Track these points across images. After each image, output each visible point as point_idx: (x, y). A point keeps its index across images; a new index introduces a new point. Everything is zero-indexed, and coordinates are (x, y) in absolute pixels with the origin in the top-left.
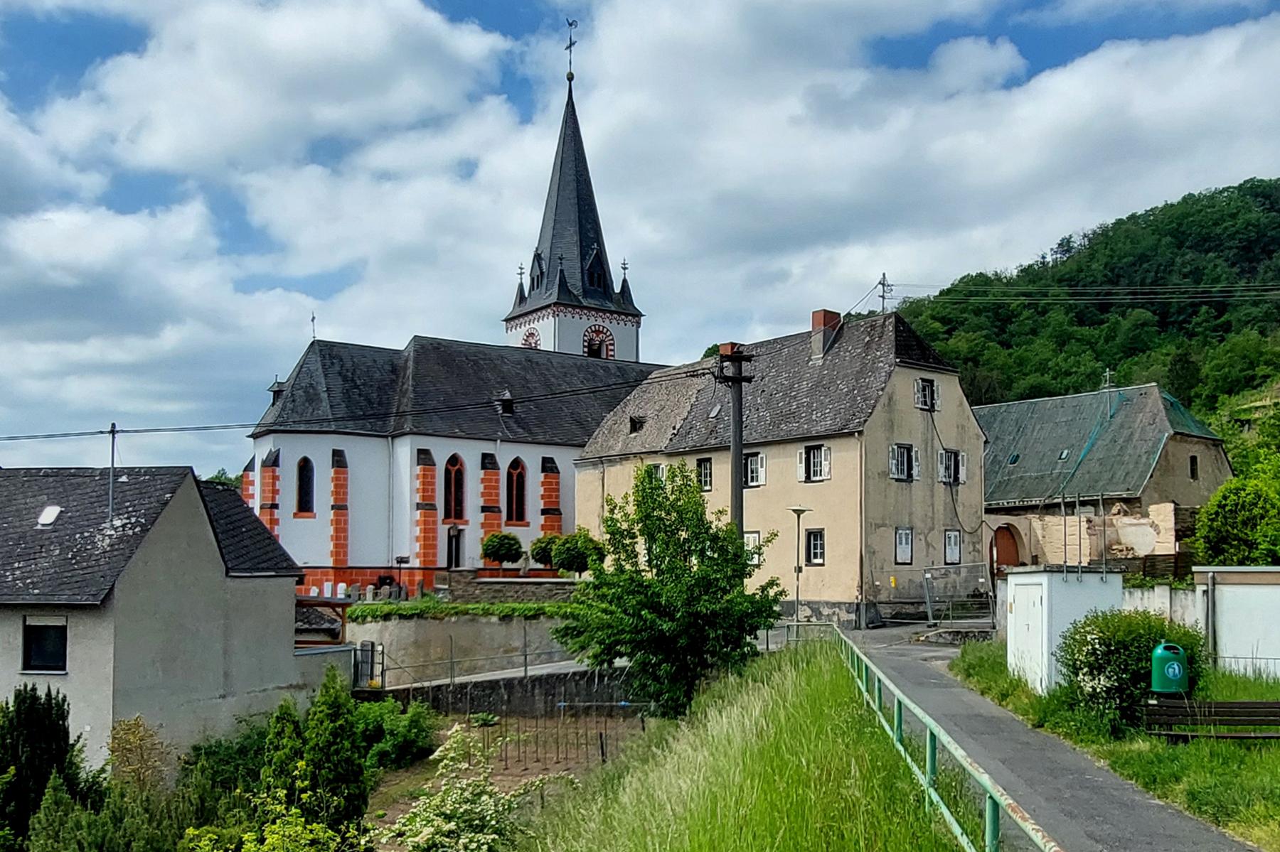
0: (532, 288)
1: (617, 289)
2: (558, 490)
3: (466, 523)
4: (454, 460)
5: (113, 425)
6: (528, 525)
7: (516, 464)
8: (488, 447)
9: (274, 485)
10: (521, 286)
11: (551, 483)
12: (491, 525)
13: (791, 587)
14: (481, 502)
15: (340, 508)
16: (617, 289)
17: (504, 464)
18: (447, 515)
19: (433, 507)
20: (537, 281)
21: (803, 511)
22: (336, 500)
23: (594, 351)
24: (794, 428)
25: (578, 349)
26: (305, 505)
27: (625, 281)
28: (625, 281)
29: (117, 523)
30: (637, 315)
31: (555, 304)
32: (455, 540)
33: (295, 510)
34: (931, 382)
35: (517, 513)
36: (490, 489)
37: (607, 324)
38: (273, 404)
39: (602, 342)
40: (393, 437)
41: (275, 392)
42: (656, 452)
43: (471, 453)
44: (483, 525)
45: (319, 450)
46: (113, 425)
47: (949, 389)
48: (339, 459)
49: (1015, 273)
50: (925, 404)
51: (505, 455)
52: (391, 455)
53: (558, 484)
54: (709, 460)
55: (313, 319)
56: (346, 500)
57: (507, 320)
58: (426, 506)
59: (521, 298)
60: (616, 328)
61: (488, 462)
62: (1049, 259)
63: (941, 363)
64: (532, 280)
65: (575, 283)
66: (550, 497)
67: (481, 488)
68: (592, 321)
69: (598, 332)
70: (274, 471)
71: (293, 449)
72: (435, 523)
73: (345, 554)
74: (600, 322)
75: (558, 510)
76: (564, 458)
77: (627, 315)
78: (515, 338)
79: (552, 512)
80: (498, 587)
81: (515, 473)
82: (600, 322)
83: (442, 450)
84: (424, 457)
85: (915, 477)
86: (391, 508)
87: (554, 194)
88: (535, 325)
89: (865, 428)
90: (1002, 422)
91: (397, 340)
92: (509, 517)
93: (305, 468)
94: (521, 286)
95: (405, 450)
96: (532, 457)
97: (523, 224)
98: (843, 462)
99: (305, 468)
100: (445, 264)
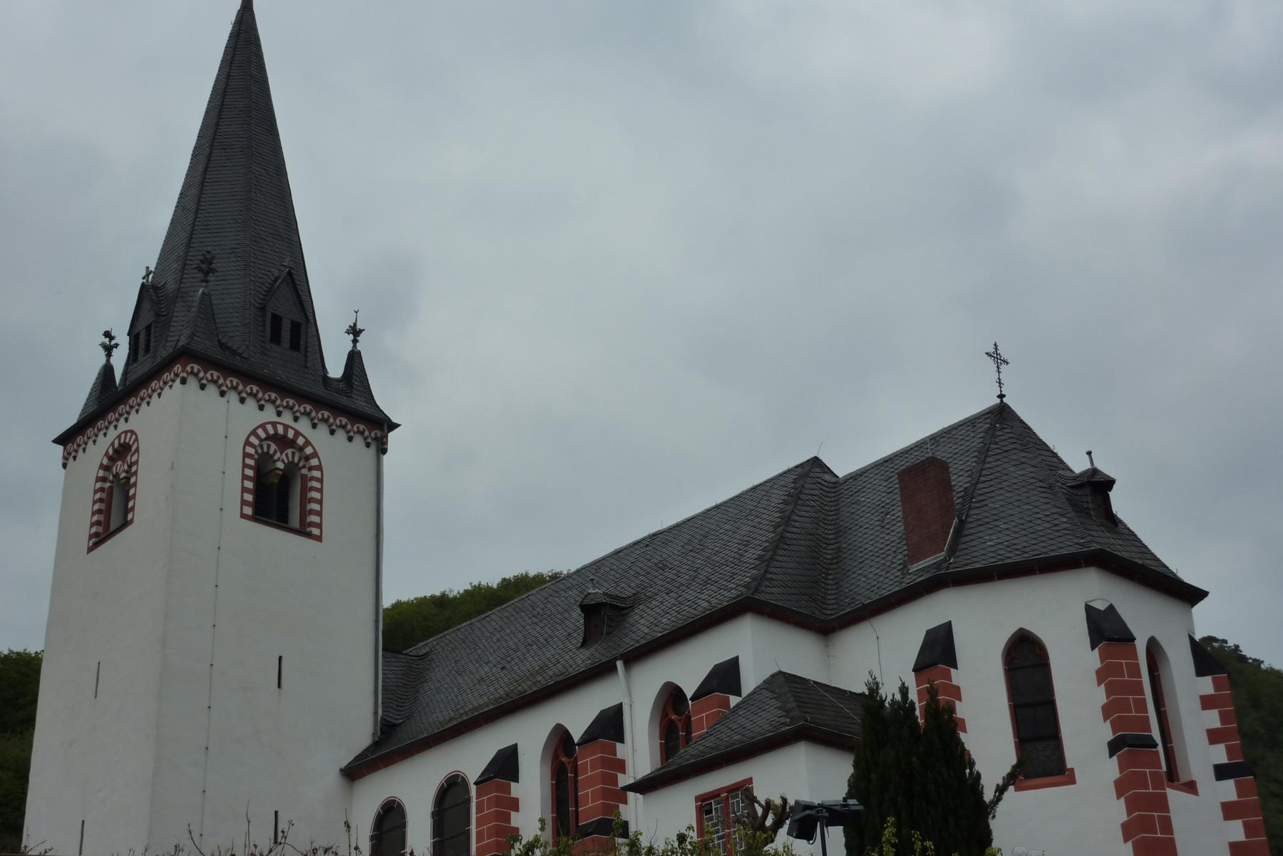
30: (376, 427)
37: (303, 426)
39: (292, 468)
68: (269, 414)
69: (283, 442)
82: (287, 418)
93: (1026, 659)
99: (1026, 659)
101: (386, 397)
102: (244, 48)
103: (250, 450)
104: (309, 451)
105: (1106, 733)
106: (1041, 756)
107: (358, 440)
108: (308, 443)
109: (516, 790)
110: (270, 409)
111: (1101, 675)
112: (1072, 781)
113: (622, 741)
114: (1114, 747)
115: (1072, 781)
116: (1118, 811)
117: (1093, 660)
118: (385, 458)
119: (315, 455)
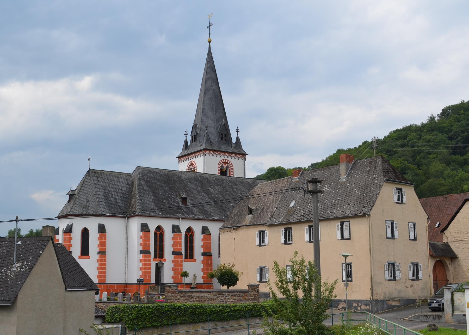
0: (192, 141)
1: (234, 141)
2: (210, 243)
3: (165, 260)
4: (159, 228)
5: (17, 217)
6: (195, 261)
7: (190, 230)
8: (176, 222)
9: (70, 242)
10: (186, 141)
11: (207, 240)
12: (178, 261)
13: (340, 293)
14: (172, 250)
15: (102, 253)
16: (234, 141)
17: (183, 230)
18: (155, 257)
19: (149, 253)
20: (194, 138)
21: (348, 256)
22: (100, 249)
23: (223, 172)
24: (336, 213)
25: (215, 171)
26: (85, 252)
27: (238, 139)
28: (238, 139)
29: (18, 265)
30: (244, 155)
31: (204, 149)
32: (159, 269)
33: (79, 254)
34: (401, 190)
35: (190, 255)
36: (176, 244)
37: (229, 159)
38: (69, 201)
39: (227, 168)
40: (128, 218)
41: (70, 196)
42: (263, 224)
43: (167, 225)
44: (173, 262)
45: (92, 224)
46: (17, 217)
47: (409, 193)
48: (102, 229)
49: (419, 124)
50: (399, 200)
51: (184, 226)
52: (127, 227)
53: (210, 240)
54: (291, 228)
55: (89, 159)
56: (105, 249)
57: (179, 157)
58: (145, 252)
59: (186, 146)
60: (235, 162)
61: (176, 229)
62: (436, 119)
63: (406, 182)
64: (192, 137)
65: (215, 138)
66: (206, 246)
67: (172, 242)
68: (222, 158)
69: (225, 163)
70: (70, 235)
71: (79, 225)
72: (150, 260)
73: (105, 277)
74: (226, 158)
75: (211, 253)
76: (214, 228)
77: (239, 154)
78: (183, 167)
79: (207, 254)
80: (189, 294)
81: (189, 235)
82: (226, 158)
83: (153, 224)
84: (144, 228)
85: (396, 237)
86: (127, 253)
87: (202, 95)
88: (194, 160)
89: (372, 213)
90: (431, 206)
91: (129, 169)
92: (186, 257)
93: (85, 233)
94: (186, 141)
95: (135, 224)
96: (197, 227)
97: (186, 109)
98: (359, 228)
99: (85, 233)
100: (150, 129)
101: (245, 148)
102: (210, 53)
103: (219, 166)
104: (230, 164)
105: (98, 250)
106: (85, 252)
107: (240, 159)
108: (230, 162)
109: (72, 235)
110: (222, 157)
111: (99, 239)
112: (89, 258)
113: (58, 234)
114: (99, 253)
115: (89, 258)
116: (97, 265)
117: (98, 235)
118: (246, 161)
119: (232, 164)
